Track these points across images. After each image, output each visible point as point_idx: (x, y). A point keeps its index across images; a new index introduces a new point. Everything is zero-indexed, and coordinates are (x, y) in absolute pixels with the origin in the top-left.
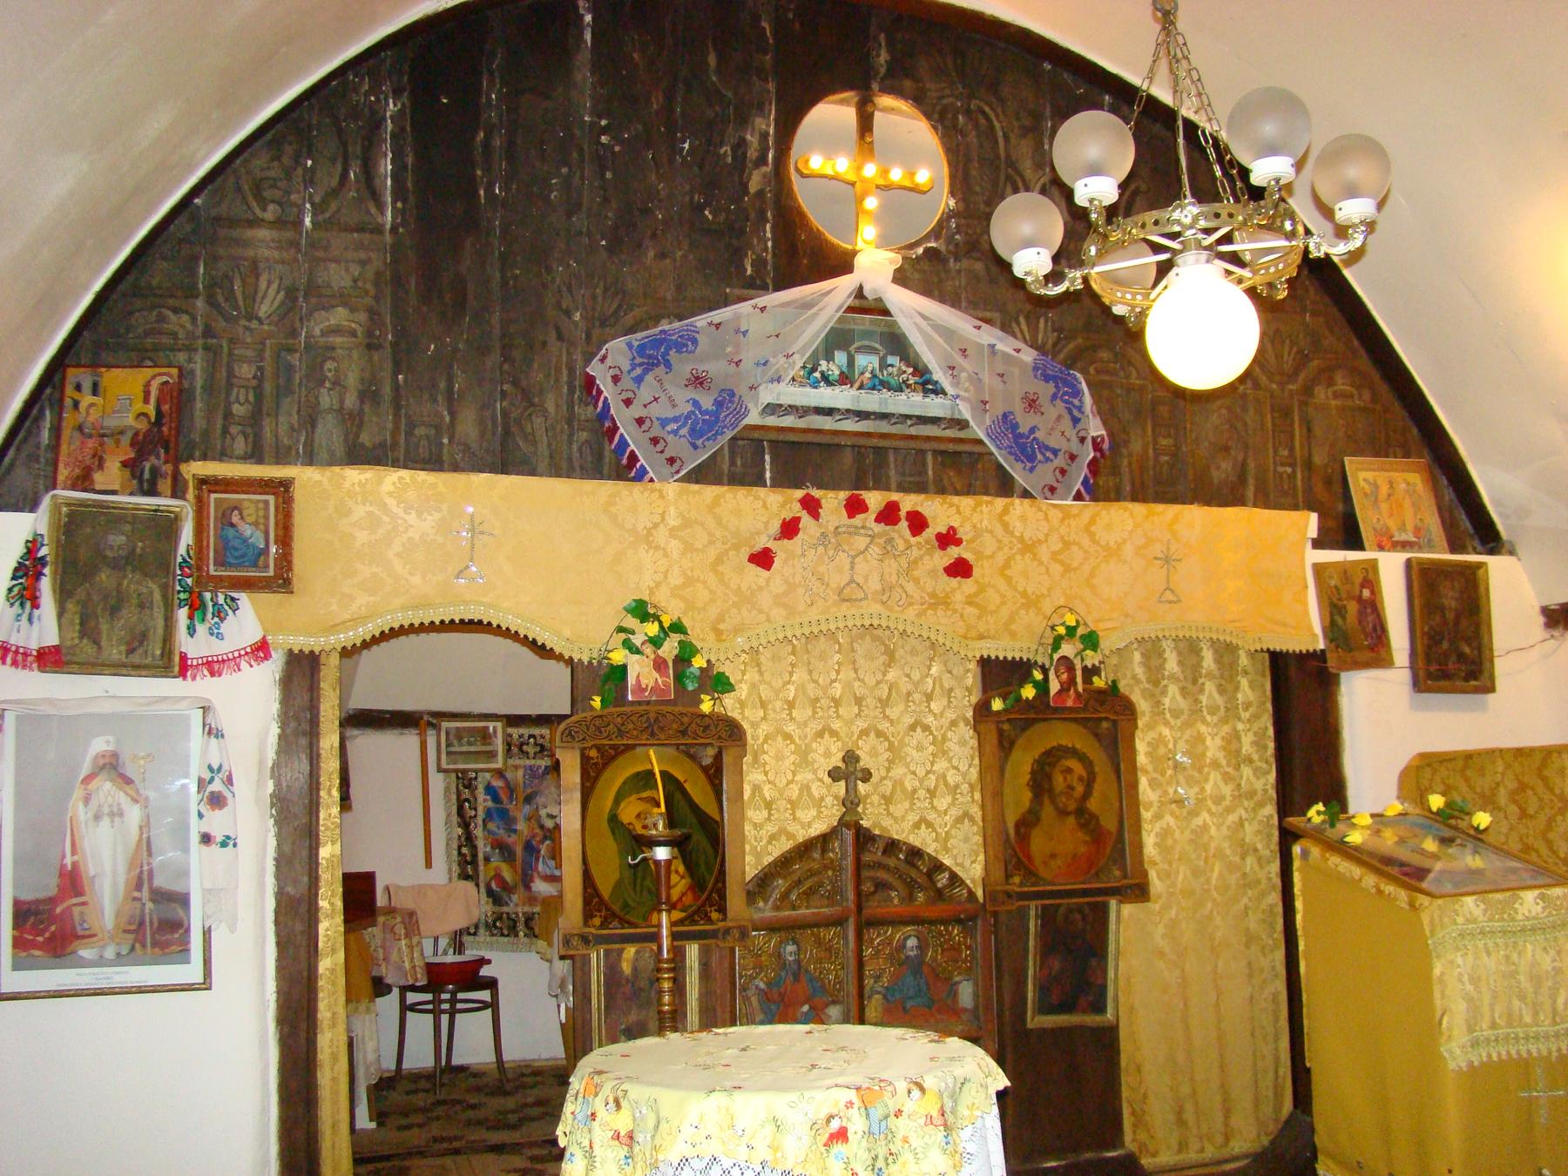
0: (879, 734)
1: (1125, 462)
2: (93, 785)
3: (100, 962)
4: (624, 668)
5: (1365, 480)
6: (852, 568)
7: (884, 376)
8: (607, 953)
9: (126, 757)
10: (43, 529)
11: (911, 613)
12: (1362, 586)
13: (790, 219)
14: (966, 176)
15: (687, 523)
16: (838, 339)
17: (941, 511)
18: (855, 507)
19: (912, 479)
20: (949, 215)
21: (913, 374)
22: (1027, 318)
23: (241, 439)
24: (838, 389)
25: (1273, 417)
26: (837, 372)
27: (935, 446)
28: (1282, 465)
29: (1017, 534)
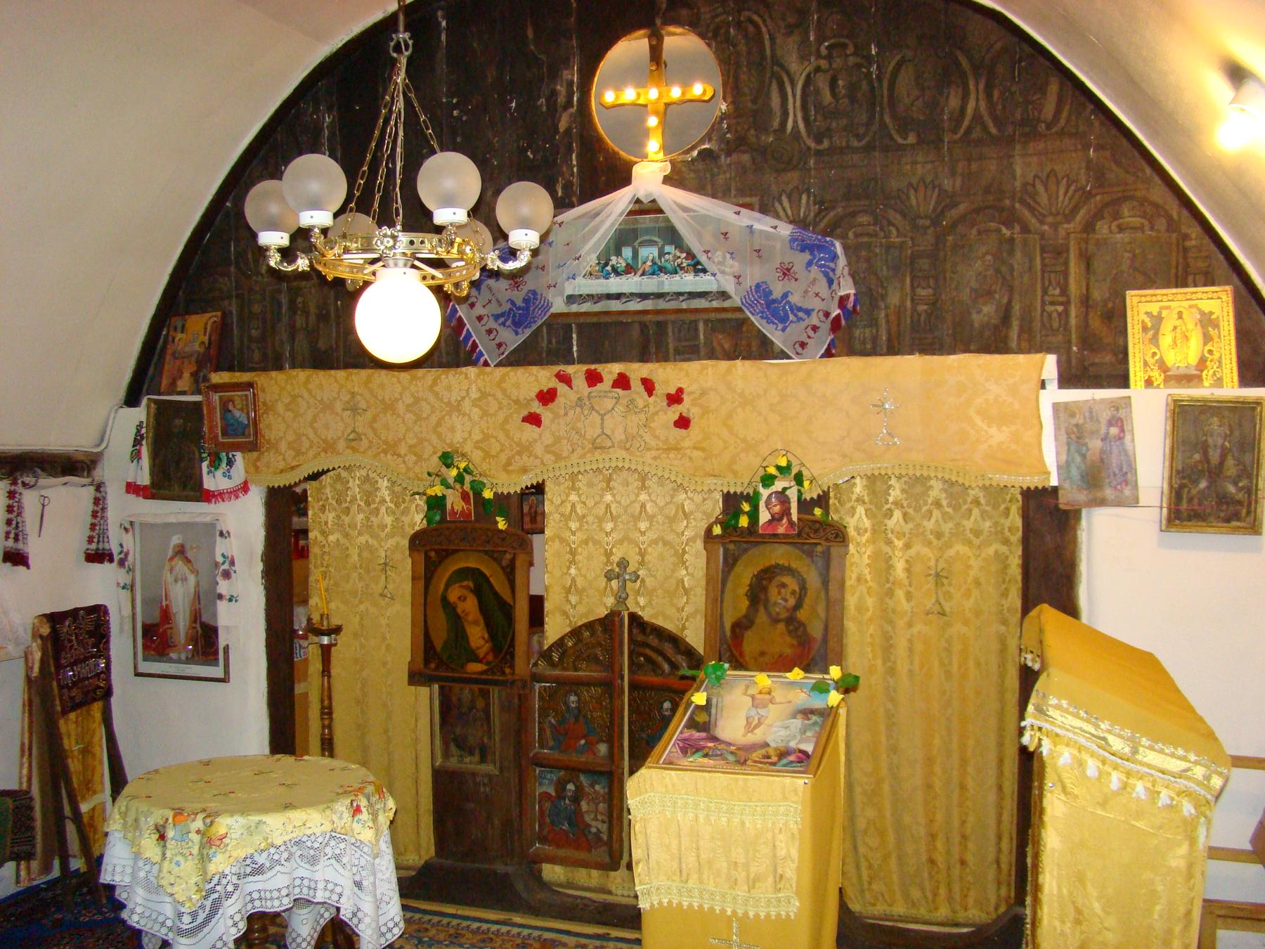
0: (666, 543)
1: (883, 314)
2: (173, 563)
3: (179, 661)
4: (444, 497)
5: (1147, 313)
6: (602, 423)
7: (663, 263)
8: (441, 688)
9: (187, 547)
10: (144, 419)
11: (648, 456)
12: (1110, 423)
13: (590, 143)
14: (736, 78)
15: (484, 395)
16: (624, 238)
17: (668, 375)
18: (593, 379)
19: (687, 344)
20: (724, 117)
21: (686, 258)
22: (789, 197)
23: (257, 351)
24: (624, 278)
25: (1043, 259)
26: (624, 265)
27: (705, 316)
28: (1052, 303)
29: (448, 441)
